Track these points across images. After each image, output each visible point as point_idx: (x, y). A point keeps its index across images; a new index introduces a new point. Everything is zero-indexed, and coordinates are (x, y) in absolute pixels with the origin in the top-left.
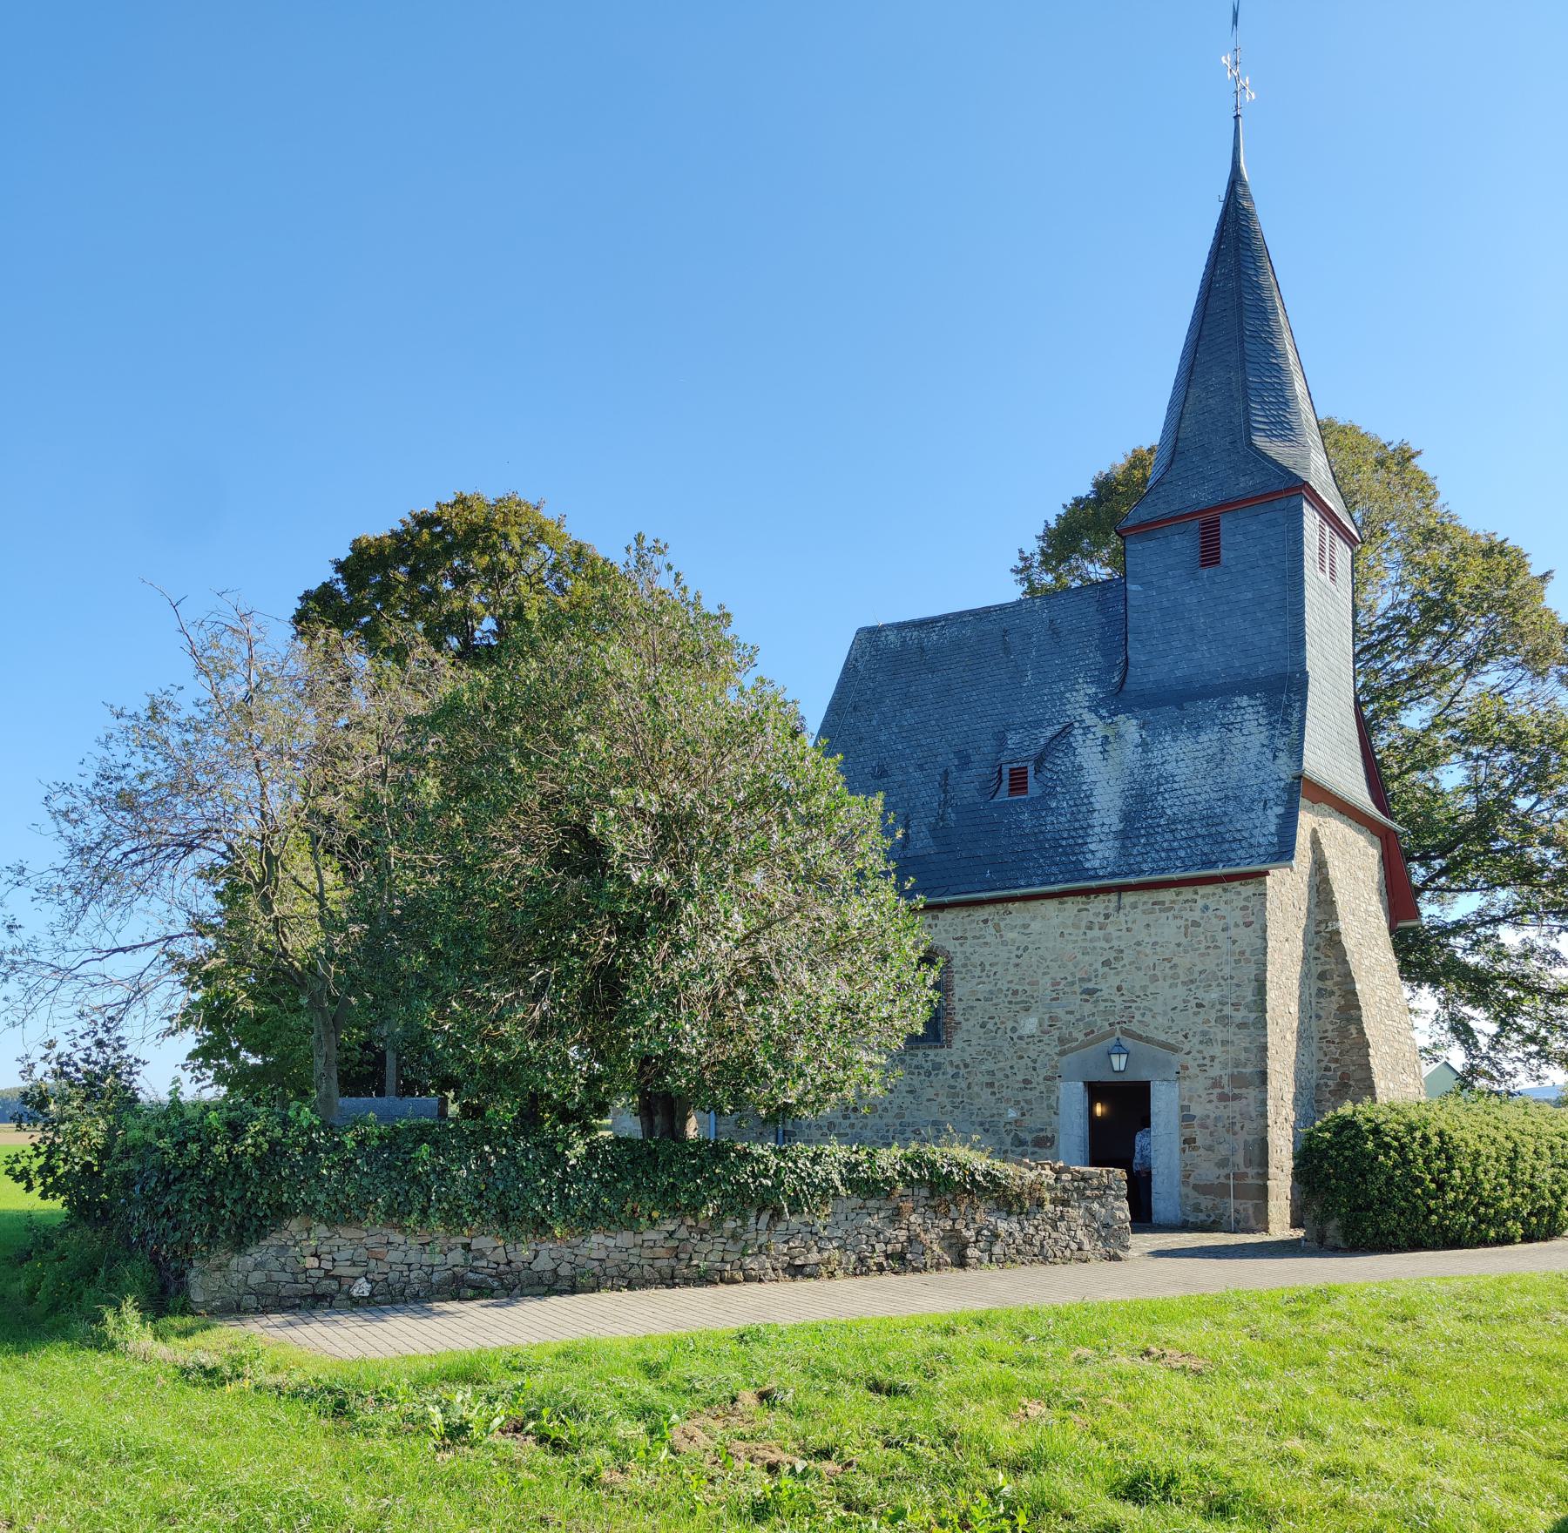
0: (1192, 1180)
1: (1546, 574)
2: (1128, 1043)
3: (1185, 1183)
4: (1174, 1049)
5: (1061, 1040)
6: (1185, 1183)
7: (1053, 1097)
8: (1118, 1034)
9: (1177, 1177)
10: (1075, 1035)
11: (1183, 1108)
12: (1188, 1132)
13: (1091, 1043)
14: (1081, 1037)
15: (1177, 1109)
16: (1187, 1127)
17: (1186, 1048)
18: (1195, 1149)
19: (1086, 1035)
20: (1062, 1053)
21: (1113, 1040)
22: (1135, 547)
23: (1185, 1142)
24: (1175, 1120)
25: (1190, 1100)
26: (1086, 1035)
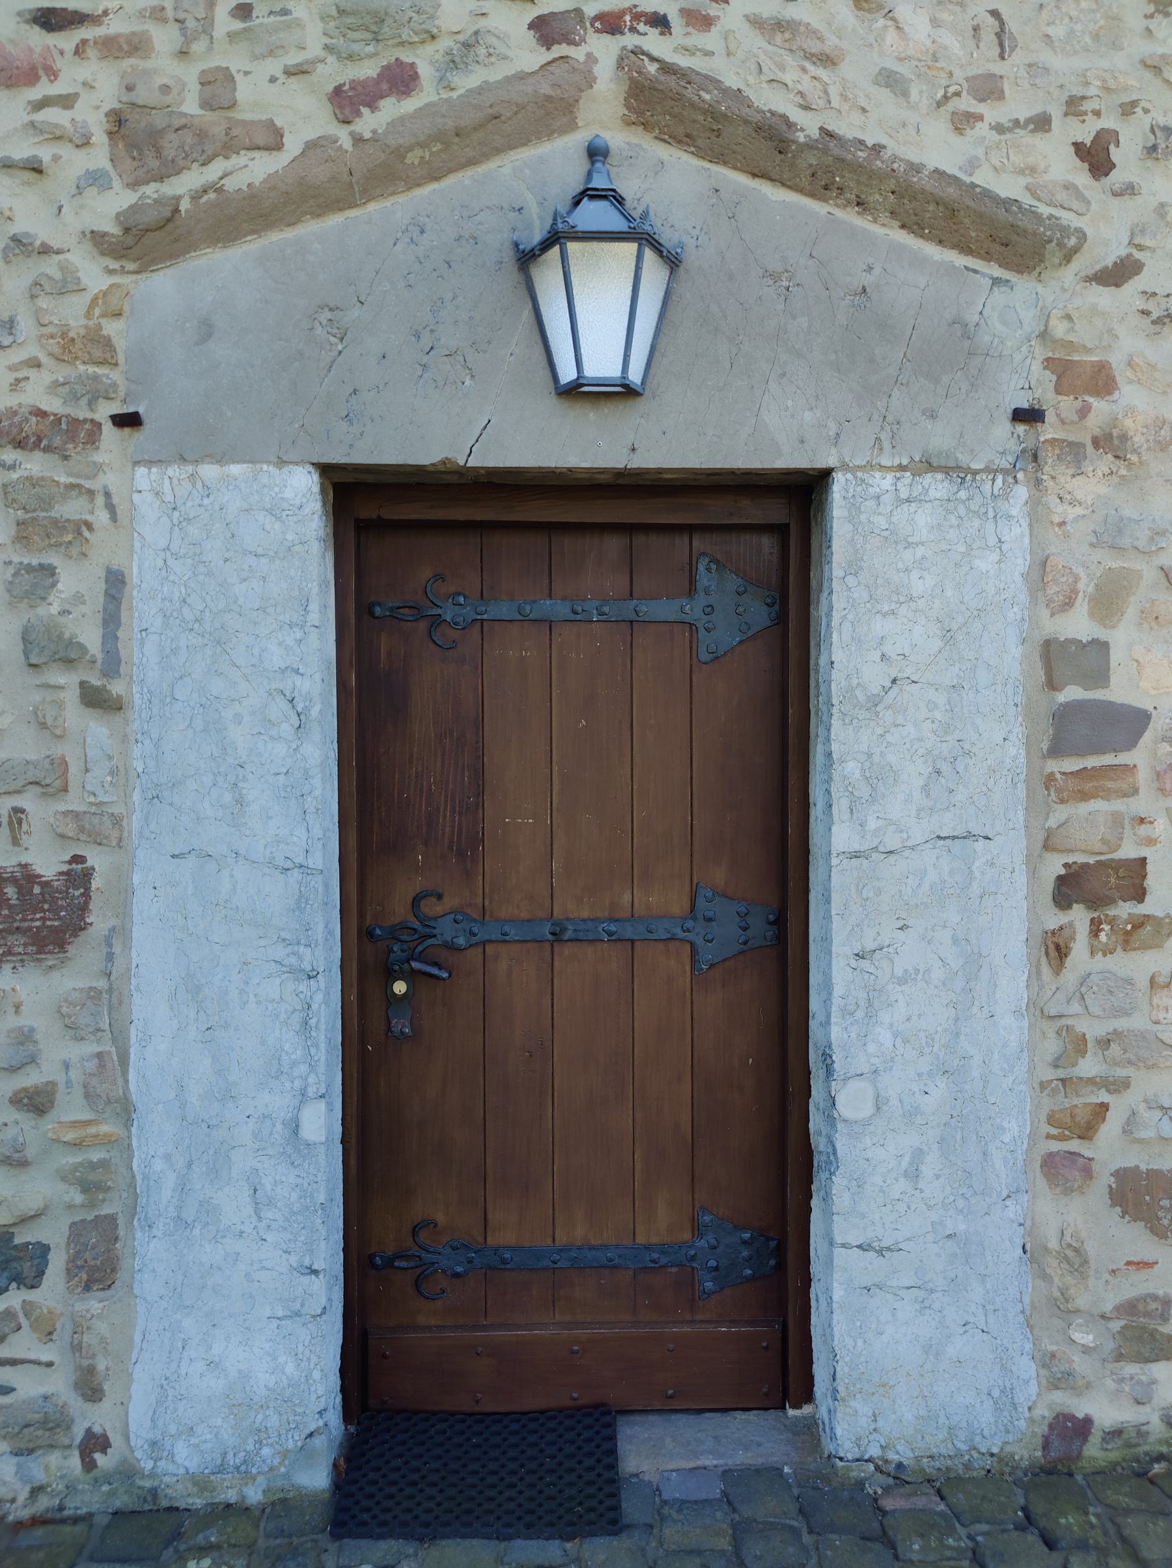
0: (1109, 1150)
1: (1146, 66)
2: (669, 180)
3: (1061, 1171)
4: (1010, 240)
5: (137, 136)
6: (1061, 1171)
7: (76, 581)
8: (602, 113)
9: (1015, 1126)
10: (258, 92)
11: (1058, 660)
12: (1090, 828)
13: (385, 171)
14: (305, 118)
15: (1008, 659)
16: (1086, 785)
17: (1107, 240)
18: (1133, 935)
19: (347, 101)
20: (145, 241)
21: (556, 161)
22: (839, 1240)
23: (1071, 887)
24: (1002, 740)
25: (1108, 600)
26: (347, 101)
